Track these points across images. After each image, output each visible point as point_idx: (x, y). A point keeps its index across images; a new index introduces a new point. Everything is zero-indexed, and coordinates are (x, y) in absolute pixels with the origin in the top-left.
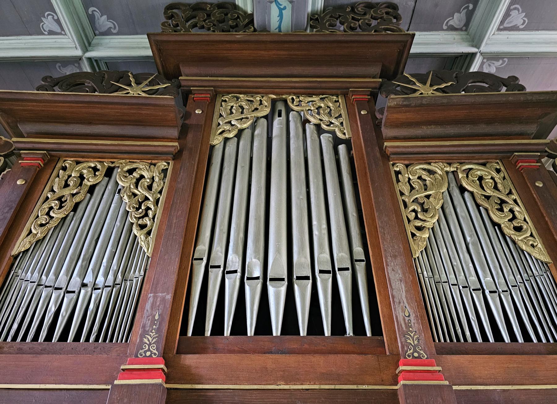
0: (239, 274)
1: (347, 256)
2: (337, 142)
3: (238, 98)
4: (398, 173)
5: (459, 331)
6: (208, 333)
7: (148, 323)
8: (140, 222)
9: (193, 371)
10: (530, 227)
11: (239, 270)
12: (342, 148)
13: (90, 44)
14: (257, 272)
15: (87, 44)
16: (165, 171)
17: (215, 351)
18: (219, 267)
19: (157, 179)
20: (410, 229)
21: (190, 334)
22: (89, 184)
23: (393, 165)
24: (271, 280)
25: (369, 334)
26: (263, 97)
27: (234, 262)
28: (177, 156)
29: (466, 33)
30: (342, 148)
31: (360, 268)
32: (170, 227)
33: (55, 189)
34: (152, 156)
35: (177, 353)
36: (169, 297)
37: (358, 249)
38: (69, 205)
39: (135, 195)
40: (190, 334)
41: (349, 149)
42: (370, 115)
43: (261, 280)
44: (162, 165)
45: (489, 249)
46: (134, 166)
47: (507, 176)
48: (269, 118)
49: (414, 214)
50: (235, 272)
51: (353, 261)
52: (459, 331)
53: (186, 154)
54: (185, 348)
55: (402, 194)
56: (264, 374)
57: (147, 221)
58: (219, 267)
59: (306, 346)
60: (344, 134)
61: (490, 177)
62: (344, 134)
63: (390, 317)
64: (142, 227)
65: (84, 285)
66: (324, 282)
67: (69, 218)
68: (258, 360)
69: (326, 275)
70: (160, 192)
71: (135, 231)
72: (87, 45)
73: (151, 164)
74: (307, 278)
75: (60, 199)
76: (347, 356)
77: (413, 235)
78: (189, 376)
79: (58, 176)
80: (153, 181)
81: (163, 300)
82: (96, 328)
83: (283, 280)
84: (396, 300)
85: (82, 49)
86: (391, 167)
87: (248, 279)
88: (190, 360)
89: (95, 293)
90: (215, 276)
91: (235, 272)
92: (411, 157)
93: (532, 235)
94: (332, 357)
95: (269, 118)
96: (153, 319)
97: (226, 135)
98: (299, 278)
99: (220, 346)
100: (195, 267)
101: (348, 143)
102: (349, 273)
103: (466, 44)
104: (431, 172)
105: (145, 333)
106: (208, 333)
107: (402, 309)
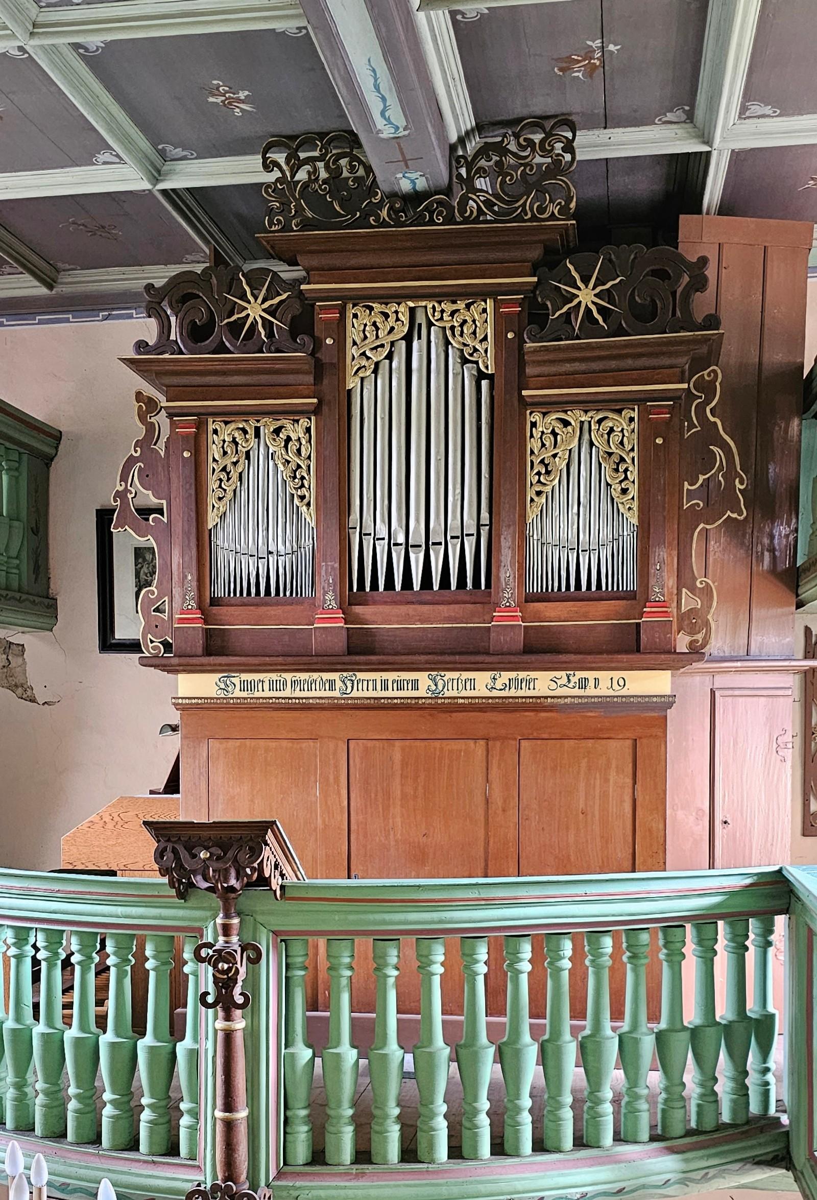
0: (386, 541)
1: (474, 523)
2: (481, 376)
3: (371, 309)
4: (534, 425)
5: (550, 583)
6: (368, 589)
7: (326, 585)
8: (299, 493)
9: (362, 617)
10: (634, 491)
11: (387, 538)
12: (484, 383)
13: (159, 172)
14: (401, 539)
15: (156, 175)
16: (308, 430)
17: (375, 603)
18: (370, 534)
19: (304, 442)
20: (530, 494)
21: (355, 590)
22: (244, 450)
23: (531, 413)
24: (412, 546)
25: (483, 587)
26: (399, 304)
27: (382, 531)
28: (317, 411)
29: (691, 125)
30: (484, 383)
31: (484, 532)
32: (325, 500)
33: (217, 458)
34: (294, 414)
35: (349, 604)
36: (337, 565)
37: (485, 515)
38: (234, 476)
39: (288, 462)
40: (355, 590)
41: (492, 387)
42: (517, 340)
43: (404, 546)
44: (304, 422)
45: (599, 506)
46: (279, 424)
47: (636, 430)
48: (408, 339)
49: (537, 477)
50: (383, 539)
51: (479, 526)
52: (550, 583)
53: (325, 409)
54: (354, 600)
55: (532, 452)
56: (408, 619)
57: (304, 491)
58: (370, 534)
59: (437, 598)
60: (487, 368)
61: (620, 429)
62: (487, 368)
63: (498, 578)
64: (302, 498)
65: (270, 553)
66: (454, 546)
67: (238, 489)
68: (403, 609)
69: (456, 540)
70: (309, 457)
71: (296, 501)
72: (156, 175)
73: (294, 420)
74: (440, 544)
75: (224, 469)
76: (463, 606)
77: (532, 500)
78: (358, 620)
79: (214, 443)
80: (301, 444)
81: (333, 568)
82: (288, 586)
83: (420, 546)
84: (503, 564)
85: (149, 181)
86: (528, 416)
87: (394, 545)
88: (358, 609)
89: (281, 559)
90: (368, 543)
91: (383, 539)
92: (546, 406)
93: (633, 498)
94: (452, 606)
95: (408, 339)
96: (329, 583)
97: (361, 374)
98: (434, 544)
99: (377, 598)
100: (351, 536)
101: (490, 377)
102: (474, 538)
103: (694, 140)
104: (566, 423)
105: (325, 593)
106: (368, 589)
107: (506, 573)
